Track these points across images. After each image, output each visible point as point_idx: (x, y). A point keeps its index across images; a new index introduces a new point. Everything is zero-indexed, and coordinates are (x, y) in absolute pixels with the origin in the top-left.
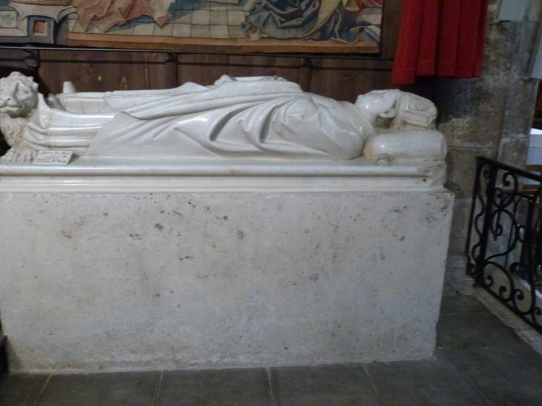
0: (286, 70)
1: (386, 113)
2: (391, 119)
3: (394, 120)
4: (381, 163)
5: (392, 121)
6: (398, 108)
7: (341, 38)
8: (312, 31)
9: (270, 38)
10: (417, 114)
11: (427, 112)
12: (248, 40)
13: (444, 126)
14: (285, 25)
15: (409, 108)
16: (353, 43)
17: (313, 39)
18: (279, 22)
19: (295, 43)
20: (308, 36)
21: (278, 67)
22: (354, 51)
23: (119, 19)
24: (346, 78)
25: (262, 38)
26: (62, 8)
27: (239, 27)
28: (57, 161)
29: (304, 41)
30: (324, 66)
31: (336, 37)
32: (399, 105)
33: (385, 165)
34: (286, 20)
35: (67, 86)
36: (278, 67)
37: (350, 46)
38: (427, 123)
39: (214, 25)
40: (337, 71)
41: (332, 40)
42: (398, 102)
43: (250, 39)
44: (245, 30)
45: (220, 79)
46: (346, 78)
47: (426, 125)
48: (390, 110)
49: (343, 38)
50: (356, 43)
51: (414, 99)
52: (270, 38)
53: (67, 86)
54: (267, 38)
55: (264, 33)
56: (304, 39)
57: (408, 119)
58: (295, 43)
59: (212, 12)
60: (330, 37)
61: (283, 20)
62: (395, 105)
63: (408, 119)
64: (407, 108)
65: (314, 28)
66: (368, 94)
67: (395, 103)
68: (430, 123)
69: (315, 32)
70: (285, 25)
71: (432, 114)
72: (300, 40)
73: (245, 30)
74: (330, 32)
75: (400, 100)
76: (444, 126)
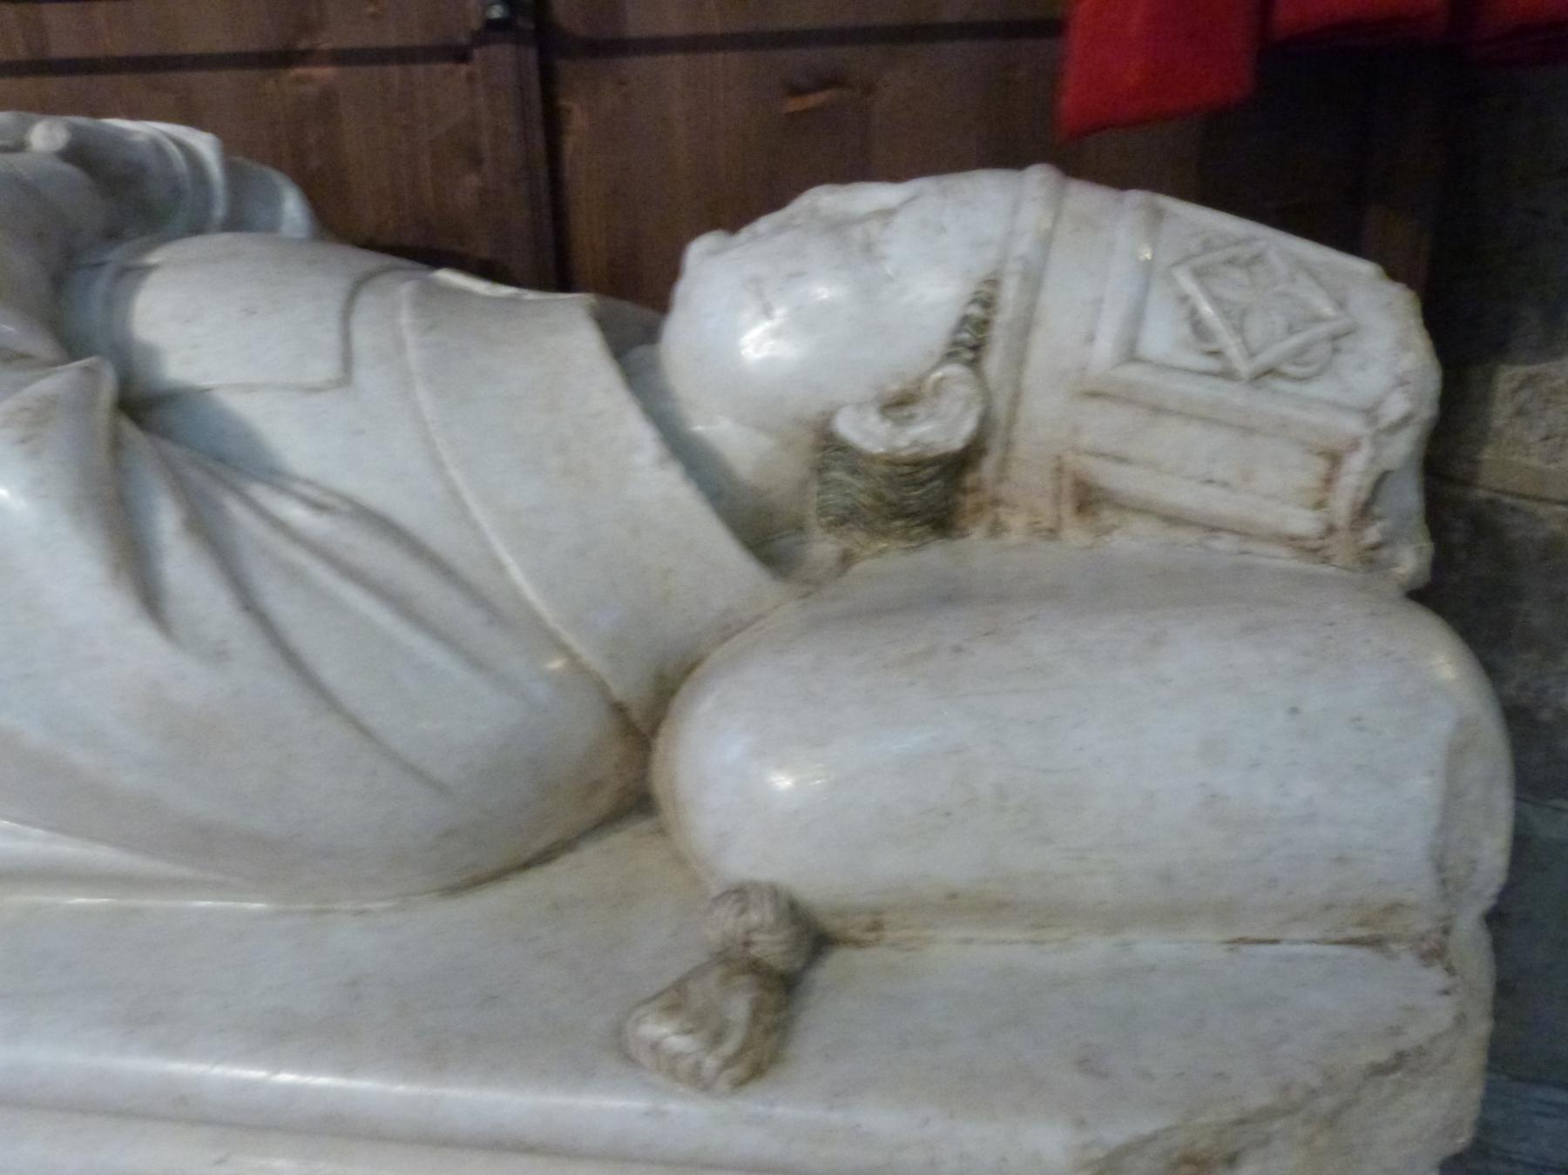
0: (394, 71)
1: (899, 404)
2: (960, 464)
3: (988, 467)
4: (655, 1047)
5: (970, 480)
6: (1019, 359)
10: (1209, 419)
11: (1314, 389)
13: (1530, 380)
15: (1131, 353)
21: (342, 57)
24: (794, 105)
32: (1026, 326)
33: (698, 1081)
36: (342, 57)
38: (1320, 505)
40: (734, 60)
42: (1010, 293)
45: (1023, 172)
46: (794, 105)
47: (1304, 522)
48: (939, 374)
51: (1187, 258)
57: (1122, 460)
62: (983, 325)
63: (1122, 460)
64: (1105, 348)
66: (764, 224)
67: (975, 311)
68: (1342, 504)
71: (1370, 413)
75: (1033, 280)
76: (1530, 380)
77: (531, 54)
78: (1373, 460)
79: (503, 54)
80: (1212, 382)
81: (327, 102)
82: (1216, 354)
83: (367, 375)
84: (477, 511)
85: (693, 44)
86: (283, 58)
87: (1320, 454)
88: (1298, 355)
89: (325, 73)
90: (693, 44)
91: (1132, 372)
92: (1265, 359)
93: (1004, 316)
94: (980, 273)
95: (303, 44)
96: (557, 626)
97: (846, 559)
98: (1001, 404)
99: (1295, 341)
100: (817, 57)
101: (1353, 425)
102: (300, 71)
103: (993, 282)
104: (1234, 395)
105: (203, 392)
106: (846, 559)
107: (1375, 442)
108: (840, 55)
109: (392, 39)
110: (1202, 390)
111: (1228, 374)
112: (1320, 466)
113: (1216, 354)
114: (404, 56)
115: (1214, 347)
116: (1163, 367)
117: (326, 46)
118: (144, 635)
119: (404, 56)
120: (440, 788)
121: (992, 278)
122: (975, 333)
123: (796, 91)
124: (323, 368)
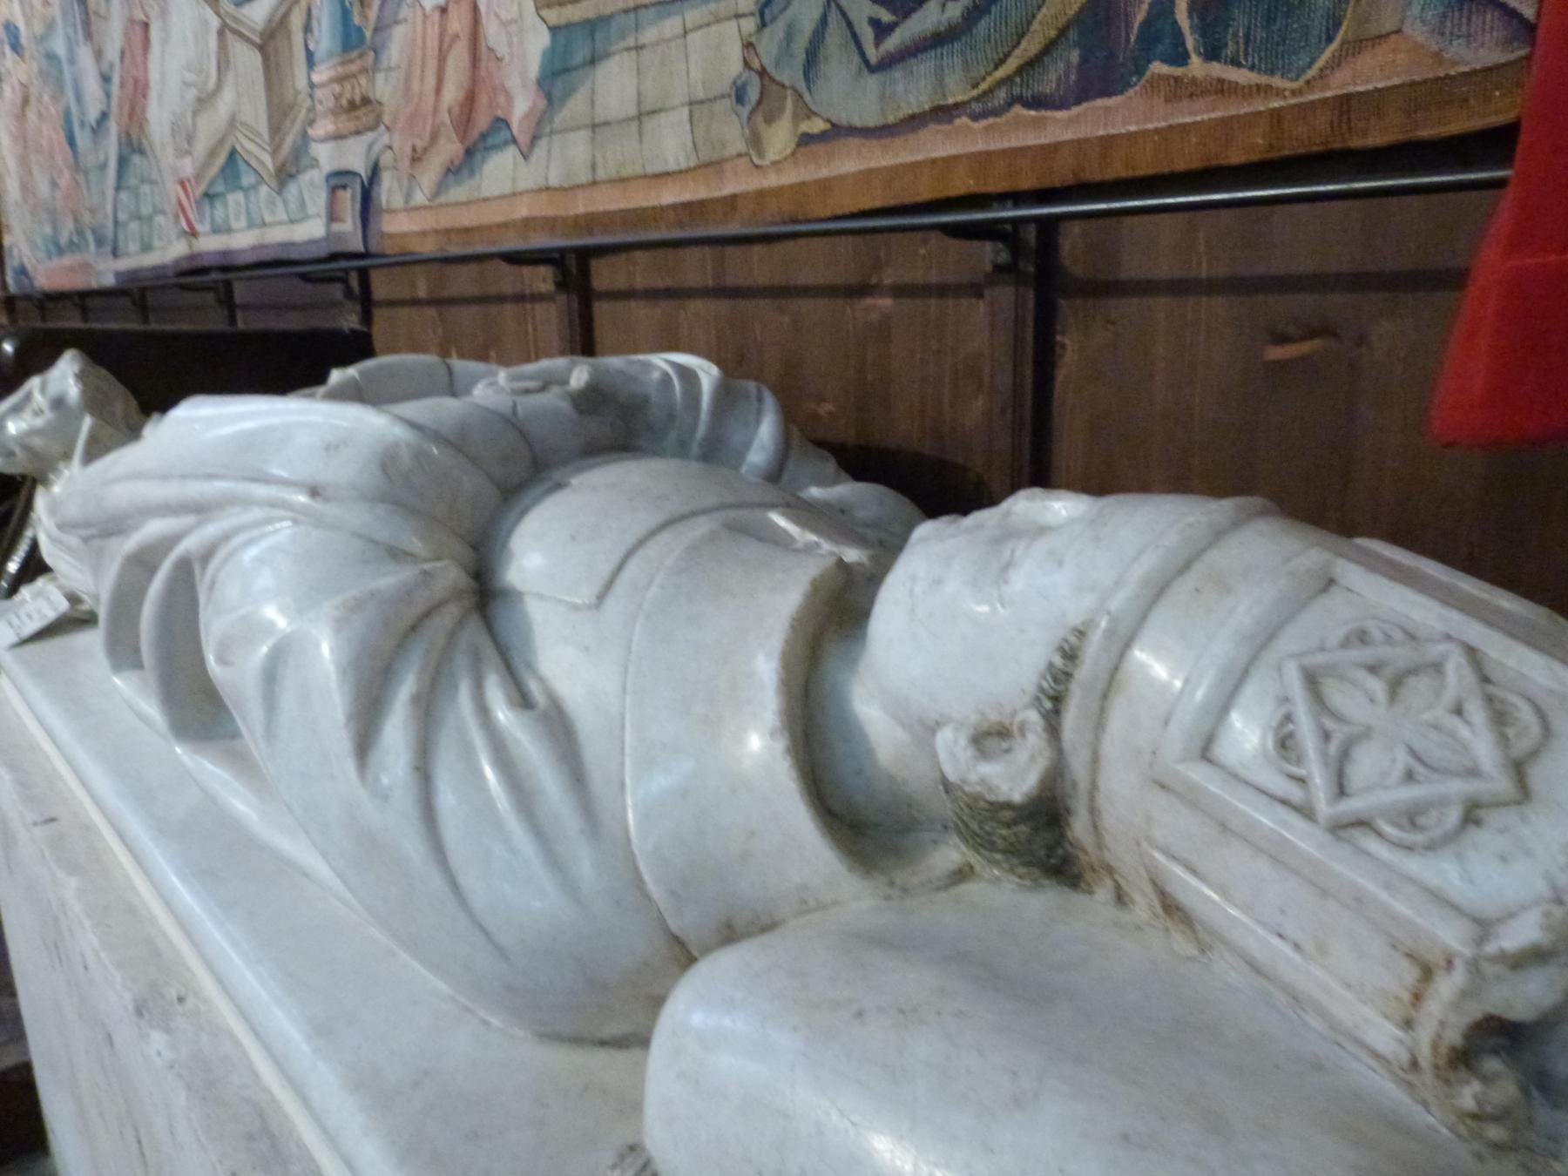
7: (1212, 53)
8: (1030, 47)
9: (838, 132)
10: (1278, 855)
11: (1413, 865)
12: (756, 160)
14: (892, 43)
16: (1300, 83)
17: (1037, 103)
18: (867, 34)
19: (936, 145)
20: (1007, 81)
21: (899, 291)
22: (1301, 139)
23: (450, 148)
24: (1276, 353)
25: (806, 140)
26: (370, 136)
27: (727, 102)
28: (62, 581)
29: (984, 123)
30: (1132, 267)
31: (1181, 58)
34: (894, 13)
35: (454, 354)
36: (899, 291)
37: (1276, 104)
39: (654, 112)
40: (1219, 305)
41: (1161, 77)
42: (1092, 652)
43: (761, 155)
44: (1256, 70)
46: (1276, 353)
49: (1230, 50)
50: (1336, 63)
52: (838, 132)
53: (454, 354)
54: (822, 137)
55: (811, 114)
56: (983, 108)
58: (936, 145)
59: (645, 53)
60: (1140, 72)
61: (886, 16)
65: (1035, 26)
69: (1048, 49)
70: (892, 43)
71: (1484, 927)
72: (963, 120)
73: (745, 111)
74: (1146, 24)
77: (1030, 297)
78: (1465, 994)
79: (1005, 294)
80: (1282, 812)
81: (882, 330)
82: (1301, 781)
83: (614, 604)
84: (628, 737)
85: (1180, 288)
86: (861, 290)
87: (1410, 956)
88: (1411, 817)
89: (886, 303)
90: (1180, 288)
91: (1198, 774)
92: (1354, 805)
93: (1083, 672)
94: (1075, 619)
95: (874, 280)
96: (637, 852)
97: (962, 874)
98: (1078, 765)
99: (1407, 794)
100: (1306, 304)
101: (1451, 936)
102: (869, 301)
103: (1081, 633)
104: (1305, 839)
105: (520, 595)
106: (962, 874)
107: (1474, 966)
108: (1337, 301)
109: (934, 277)
110: (1267, 818)
111: (1306, 811)
112: (1410, 974)
113: (1301, 781)
114: (942, 291)
115: (1301, 772)
116: (1235, 777)
117: (887, 281)
118: (350, 765)
119: (942, 291)
120: (501, 952)
121: (1081, 628)
122: (1052, 684)
123: (1282, 339)
124: (586, 594)
